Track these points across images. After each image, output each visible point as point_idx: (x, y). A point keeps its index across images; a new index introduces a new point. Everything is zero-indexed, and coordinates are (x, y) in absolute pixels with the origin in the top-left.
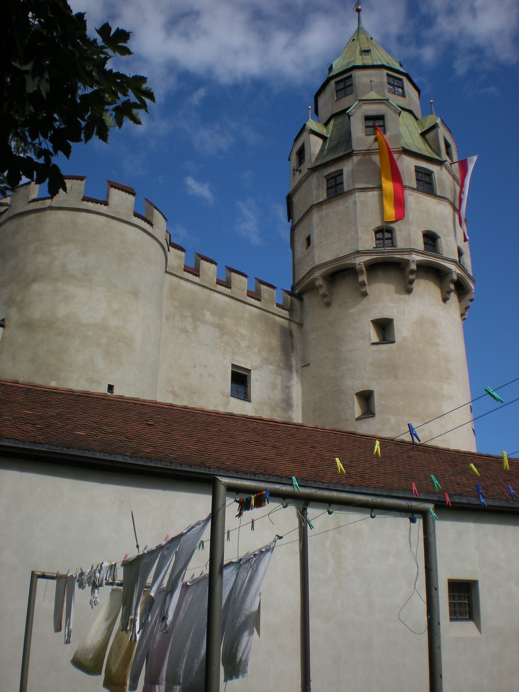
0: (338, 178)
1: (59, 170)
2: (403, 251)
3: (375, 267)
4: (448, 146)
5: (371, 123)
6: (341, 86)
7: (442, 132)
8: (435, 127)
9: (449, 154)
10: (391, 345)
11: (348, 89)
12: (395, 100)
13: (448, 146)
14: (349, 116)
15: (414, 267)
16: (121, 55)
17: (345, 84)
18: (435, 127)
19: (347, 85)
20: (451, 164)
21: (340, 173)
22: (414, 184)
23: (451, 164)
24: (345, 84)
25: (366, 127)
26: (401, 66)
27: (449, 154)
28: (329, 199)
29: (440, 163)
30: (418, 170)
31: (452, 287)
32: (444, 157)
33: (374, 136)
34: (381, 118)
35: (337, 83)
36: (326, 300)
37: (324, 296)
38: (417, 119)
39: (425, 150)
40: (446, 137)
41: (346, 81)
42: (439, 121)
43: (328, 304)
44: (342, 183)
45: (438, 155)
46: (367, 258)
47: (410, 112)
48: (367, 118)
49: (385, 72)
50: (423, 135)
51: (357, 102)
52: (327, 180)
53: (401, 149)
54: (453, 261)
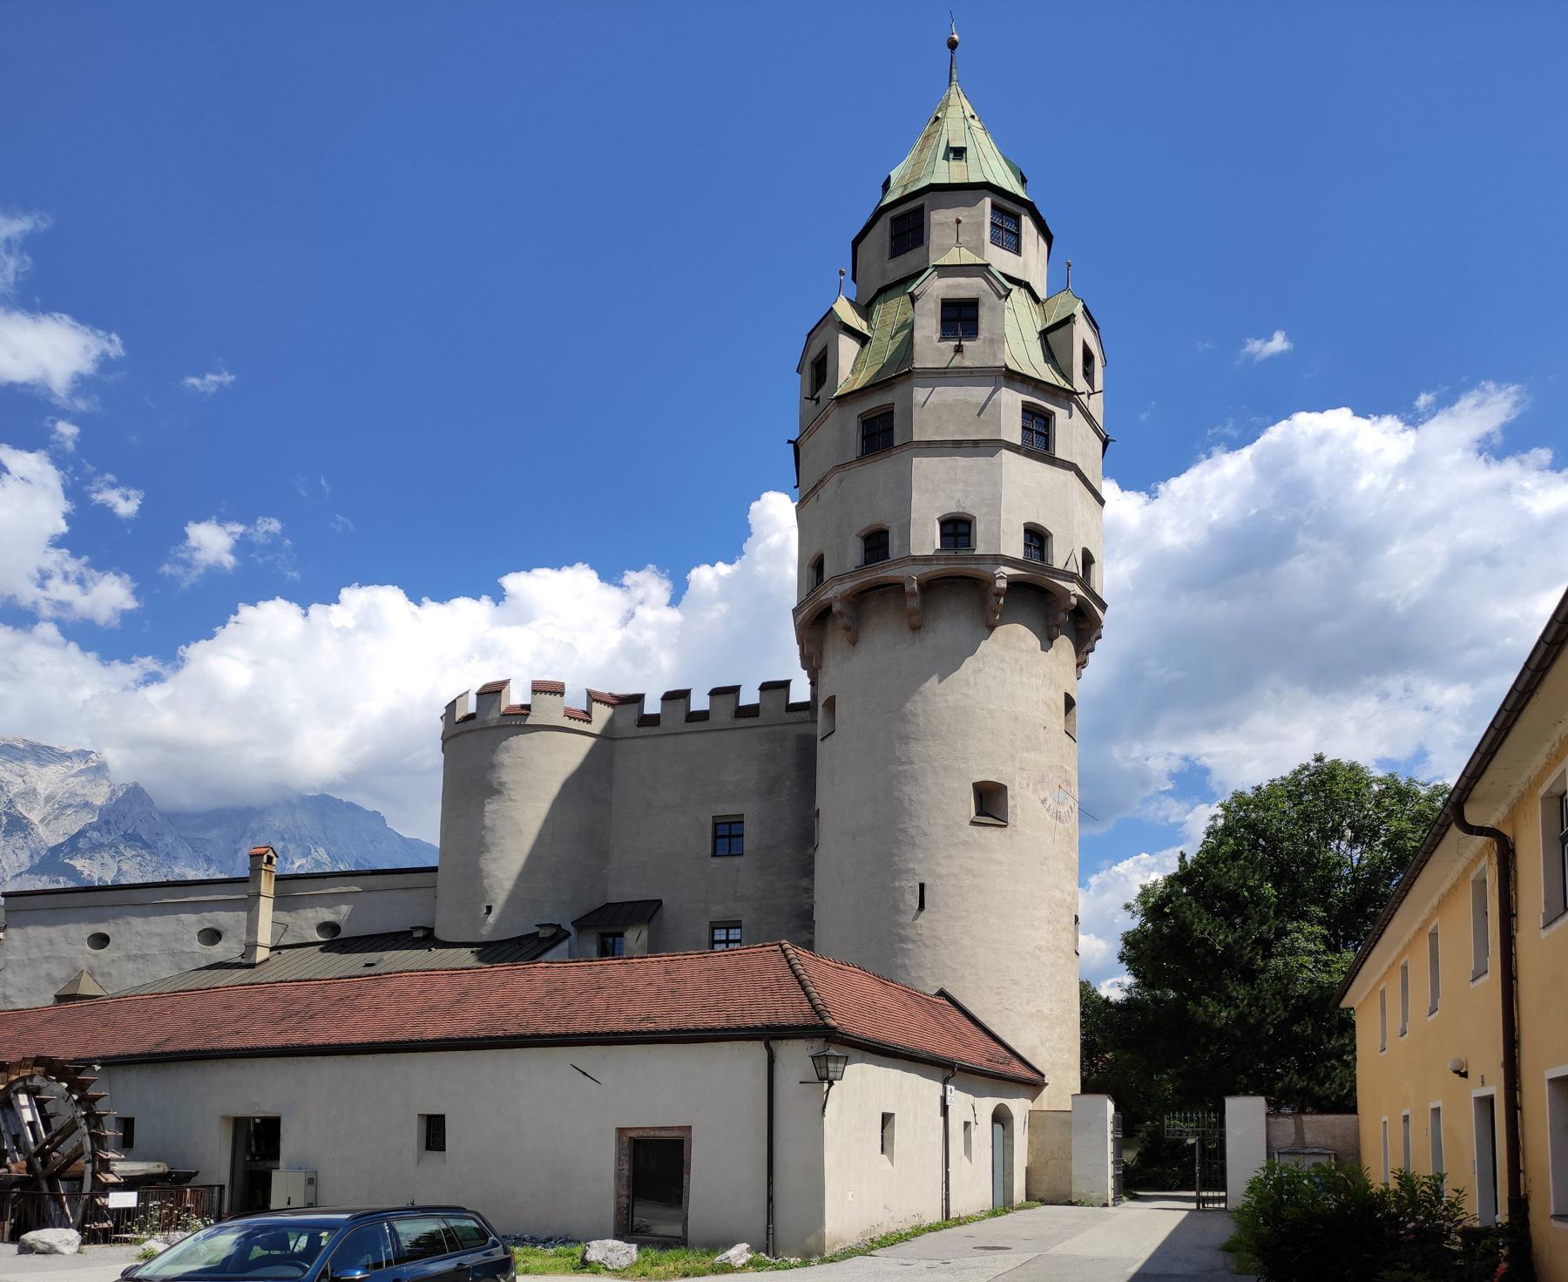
1: (1178, 475)
2: (982, 558)
4: (1088, 357)
7: (1082, 331)
8: (1068, 320)
9: (1088, 374)
10: (737, 859)
12: (1000, 260)
13: (1088, 357)
14: (913, 299)
15: (1002, 584)
18: (1068, 320)
22: (1016, 437)
26: (1023, 181)
27: (1088, 374)
30: (1029, 411)
31: (1064, 617)
32: (1080, 384)
35: (893, 220)
38: (1036, 299)
39: (1047, 374)
42: (1078, 309)
43: (915, 628)
45: (1064, 376)
46: (849, 585)
47: (1026, 286)
54: (1071, 577)
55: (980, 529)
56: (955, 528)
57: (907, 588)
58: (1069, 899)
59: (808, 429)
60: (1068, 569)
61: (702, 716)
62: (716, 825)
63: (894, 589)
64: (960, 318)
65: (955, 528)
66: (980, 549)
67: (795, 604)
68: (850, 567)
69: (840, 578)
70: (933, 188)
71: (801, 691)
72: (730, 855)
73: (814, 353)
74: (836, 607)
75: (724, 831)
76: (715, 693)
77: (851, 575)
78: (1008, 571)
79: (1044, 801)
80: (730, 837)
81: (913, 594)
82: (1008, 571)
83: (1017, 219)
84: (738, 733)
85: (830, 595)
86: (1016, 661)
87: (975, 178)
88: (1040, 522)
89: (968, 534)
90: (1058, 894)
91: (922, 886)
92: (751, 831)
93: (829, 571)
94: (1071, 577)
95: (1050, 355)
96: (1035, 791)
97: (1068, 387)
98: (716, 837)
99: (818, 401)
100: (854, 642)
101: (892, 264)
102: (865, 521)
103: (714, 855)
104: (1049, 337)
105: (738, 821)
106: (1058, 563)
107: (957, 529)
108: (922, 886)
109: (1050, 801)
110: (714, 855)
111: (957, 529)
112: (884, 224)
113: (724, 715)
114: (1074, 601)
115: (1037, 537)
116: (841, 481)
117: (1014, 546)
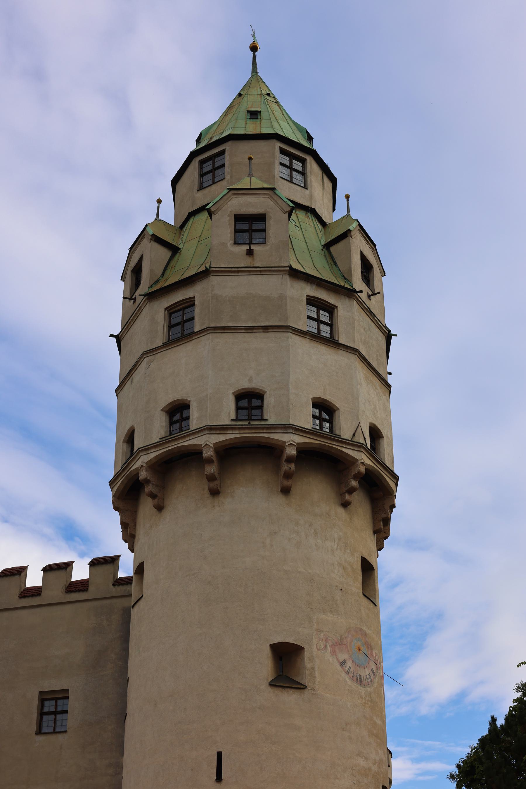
0: (186, 311)
3: (232, 455)
5: (245, 226)
6: (208, 167)
10: (60, 737)
11: (217, 173)
15: (293, 452)
16: (171, 181)
17: (214, 164)
19: (217, 165)
20: (369, 296)
21: (190, 303)
23: (369, 296)
24: (214, 164)
25: (236, 231)
28: (171, 342)
29: (351, 293)
32: (358, 283)
33: (246, 247)
34: (262, 218)
35: (202, 162)
36: (213, 485)
37: (211, 478)
40: (365, 253)
41: (216, 160)
43: (215, 493)
44: (193, 319)
46: (153, 455)
48: (239, 218)
49: (278, 145)
50: (327, 246)
51: (226, 191)
52: (170, 314)
53: (288, 269)
54: (360, 446)
55: (269, 401)
56: (250, 402)
57: (204, 455)
58: (374, 768)
59: (127, 325)
60: (356, 439)
61: (36, 591)
62: (42, 702)
63: (192, 457)
64: (251, 227)
65: (250, 402)
66: (272, 420)
67: (111, 476)
68: (155, 439)
69: (146, 449)
70: (232, 137)
71: (126, 569)
72: (54, 732)
73: (133, 263)
74: (143, 475)
75: (49, 706)
76: (47, 570)
77: (156, 446)
78: (298, 439)
79: (343, 664)
80: (55, 713)
81: (210, 461)
82: (298, 439)
83: (303, 161)
84: (68, 607)
85: (138, 465)
86: (311, 525)
87: (266, 130)
88: (328, 397)
89: (261, 408)
90: (361, 762)
91: (219, 755)
92: (74, 705)
93: (138, 443)
94: (360, 446)
95: (333, 261)
96: (333, 653)
97: (347, 286)
98: (42, 714)
99: (135, 300)
100: (160, 508)
101: (200, 194)
102: (167, 398)
103: (39, 732)
104: (332, 249)
105: (63, 695)
106: (346, 435)
107: (249, 401)
108: (219, 755)
109: (349, 664)
110: (39, 732)
111: (249, 401)
112: (195, 164)
113: (56, 593)
114: (362, 469)
115: (324, 409)
116: (150, 363)
117: (305, 418)
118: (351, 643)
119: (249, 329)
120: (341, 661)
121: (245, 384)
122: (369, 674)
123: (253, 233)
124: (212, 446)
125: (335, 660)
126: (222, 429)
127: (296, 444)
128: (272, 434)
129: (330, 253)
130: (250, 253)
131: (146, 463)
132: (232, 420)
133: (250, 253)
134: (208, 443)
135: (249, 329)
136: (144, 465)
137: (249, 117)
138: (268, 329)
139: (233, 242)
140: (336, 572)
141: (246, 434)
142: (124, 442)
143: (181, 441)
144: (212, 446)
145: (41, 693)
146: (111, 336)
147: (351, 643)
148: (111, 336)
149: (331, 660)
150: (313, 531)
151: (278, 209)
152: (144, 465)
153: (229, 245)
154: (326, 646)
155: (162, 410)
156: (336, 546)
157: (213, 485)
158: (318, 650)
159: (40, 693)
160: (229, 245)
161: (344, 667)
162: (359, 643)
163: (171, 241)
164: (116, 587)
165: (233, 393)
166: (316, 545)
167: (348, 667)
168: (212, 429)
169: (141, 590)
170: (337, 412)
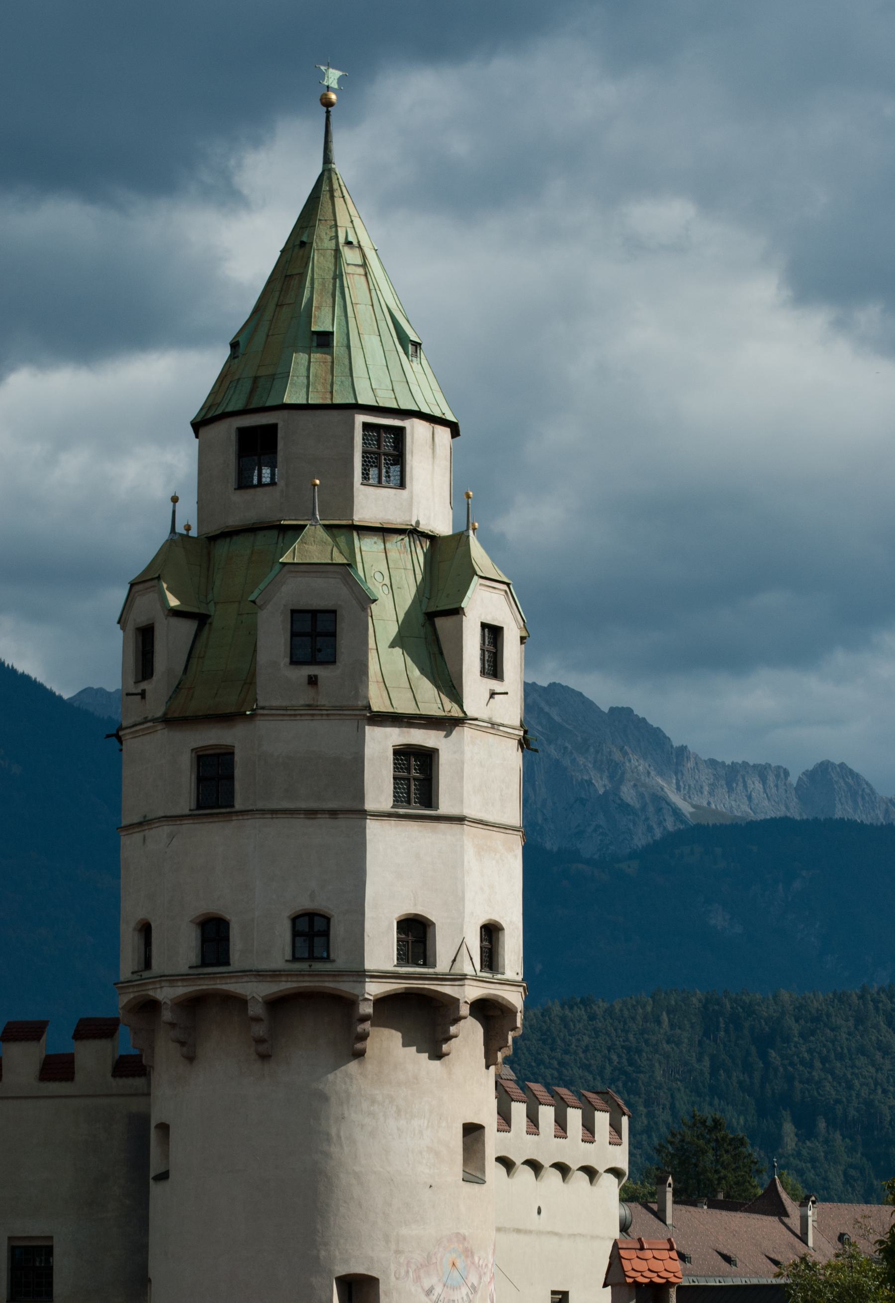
36: (263, 1048)
37: (259, 1041)
79: (429, 1292)
101: (240, 498)
116: (172, 836)
118: (441, 1259)
119: (311, 813)
120: (427, 1288)
121: (305, 904)
122: (467, 1294)
123: (318, 638)
124: (260, 1000)
125: (420, 1290)
126: (275, 975)
127: (371, 998)
128: (341, 984)
129: (433, 625)
130: (313, 681)
131: (171, 1000)
132: (287, 961)
133: (313, 681)
134: (255, 995)
135: (311, 813)
136: (169, 1003)
137: (315, 344)
138: (336, 814)
139: (288, 660)
140: (424, 1162)
141: (307, 984)
142: (134, 929)
143: (218, 982)
144: (260, 1000)
145: (10, 1238)
146: (108, 736)
147: (441, 1259)
148: (108, 736)
149: (413, 1289)
150: (394, 1108)
151: (354, 602)
152: (169, 1003)
153: (282, 665)
154: (408, 1272)
155: (191, 921)
156: (425, 1125)
157: (263, 1048)
158: (397, 1279)
159: (10, 1238)
160: (282, 665)
161: (431, 1296)
162: (454, 1255)
163: (196, 610)
164: (117, 1079)
165: (289, 917)
166: (398, 1129)
167: (436, 1294)
168: (260, 975)
169: (166, 1155)
170: (431, 927)
